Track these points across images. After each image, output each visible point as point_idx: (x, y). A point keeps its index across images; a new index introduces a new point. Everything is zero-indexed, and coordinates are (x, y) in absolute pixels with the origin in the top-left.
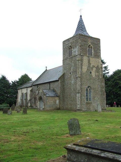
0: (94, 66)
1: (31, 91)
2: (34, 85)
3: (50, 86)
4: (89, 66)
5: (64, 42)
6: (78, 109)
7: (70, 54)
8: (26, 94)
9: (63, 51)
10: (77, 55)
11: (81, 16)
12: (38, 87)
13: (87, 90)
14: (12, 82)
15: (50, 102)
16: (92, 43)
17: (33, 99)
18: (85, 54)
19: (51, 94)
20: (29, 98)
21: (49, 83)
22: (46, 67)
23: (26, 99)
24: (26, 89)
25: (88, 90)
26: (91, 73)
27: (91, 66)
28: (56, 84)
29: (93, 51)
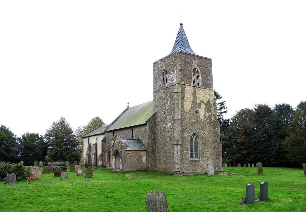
1: (104, 141)
2: (107, 132)
4: (194, 102)
6: (177, 170)
8: (96, 145)
10: (175, 84)
11: (181, 24)
12: (114, 134)
13: (191, 139)
15: (132, 159)
20: (99, 152)
21: (132, 128)
23: (95, 154)
26: (197, 112)
27: (198, 101)
28: (143, 129)
29: (200, 78)
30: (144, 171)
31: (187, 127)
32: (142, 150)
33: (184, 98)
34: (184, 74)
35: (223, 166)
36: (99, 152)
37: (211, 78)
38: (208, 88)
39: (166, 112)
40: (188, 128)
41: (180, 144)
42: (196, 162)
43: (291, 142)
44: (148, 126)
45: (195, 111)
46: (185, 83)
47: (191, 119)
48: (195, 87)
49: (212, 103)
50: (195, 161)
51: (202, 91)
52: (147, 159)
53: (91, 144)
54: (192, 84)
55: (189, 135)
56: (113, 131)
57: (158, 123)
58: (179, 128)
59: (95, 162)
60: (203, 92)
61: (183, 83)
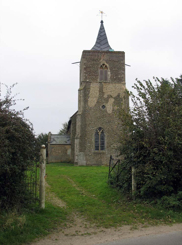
0: (110, 96)
11: (102, 22)
13: (97, 133)
14: (163, 79)
15: (57, 151)
18: (95, 80)
26: (104, 107)
27: (105, 96)
29: (109, 73)
30: (68, 162)
31: (91, 122)
32: (67, 144)
33: (88, 94)
37: (123, 72)
38: (119, 82)
40: (92, 123)
42: (100, 154)
45: (101, 106)
46: (90, 80)
48: (103, 83)
49: (123, 97)
50: (100, 154)
51: (111, 86)
54: (98, 80)
55: (94, 129)
58: (79, 123)
60: (112, 87)
61: (88, 80)
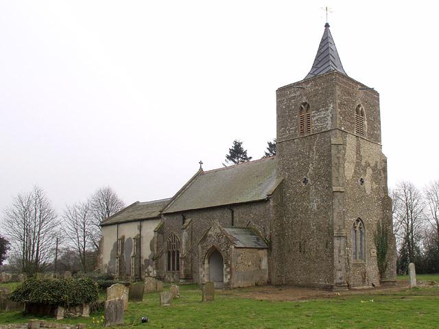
1: (160, 231)
2: (165, 215)
3: (233, 215)
4: (358, 164)
5: (283, 93)
6: (340, 281)
7: (305, 124)
8: (138, 240)
9: (278, 117)
10: (329, 129)
11: (327, 26)
12: (184, 219)
15: (246, 263)
16: (365, 102)
17: (165, 256)
19: (243, 240)
20: (146, 253)
21: (231, 207)
22: (201, 163)
23: (138, 256)
24: (136, 225)
25: (357, 229)
26: (362, 181)
27: (363, 163)
28: (260, 209)
29: (366, 123)
34: (344, 112)
35: (397, 273)
36: (146, 253)
39: (309, 179)
41: (345, 235)
43: (190, 279)
44: (271, 204)
47: (354, 194)
52: (269, 262)
53: (124, 237)
56: (184, 214)
57: (290, 198)
59: (137, 273)
